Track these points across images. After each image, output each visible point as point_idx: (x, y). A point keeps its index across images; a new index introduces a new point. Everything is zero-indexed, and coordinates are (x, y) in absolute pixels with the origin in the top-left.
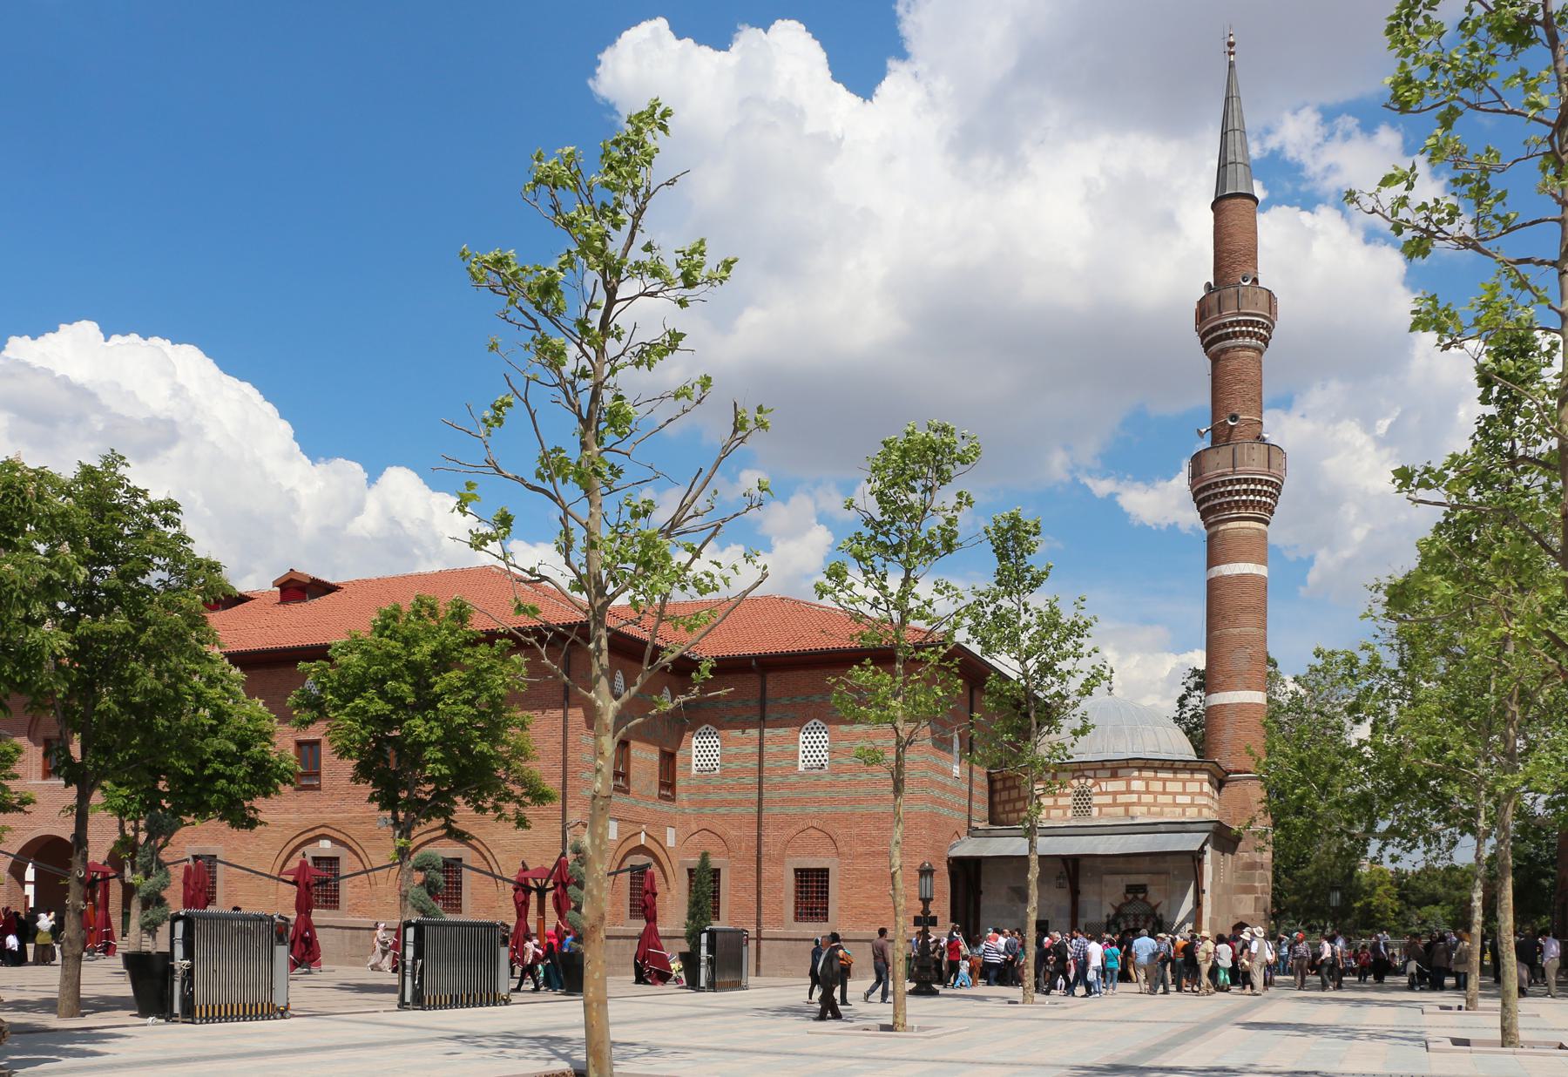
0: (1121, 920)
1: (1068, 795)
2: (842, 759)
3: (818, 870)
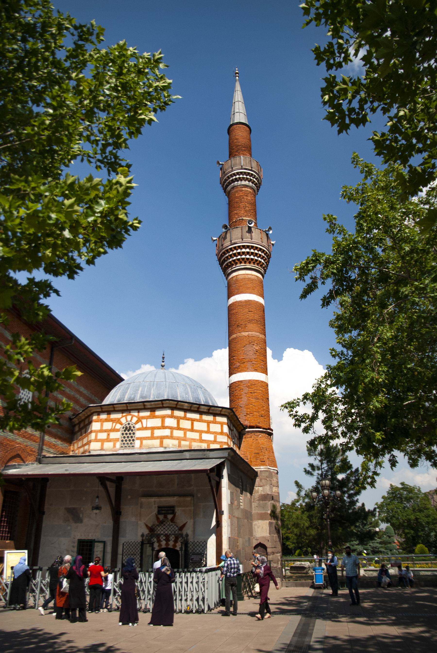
1: (118, 430)
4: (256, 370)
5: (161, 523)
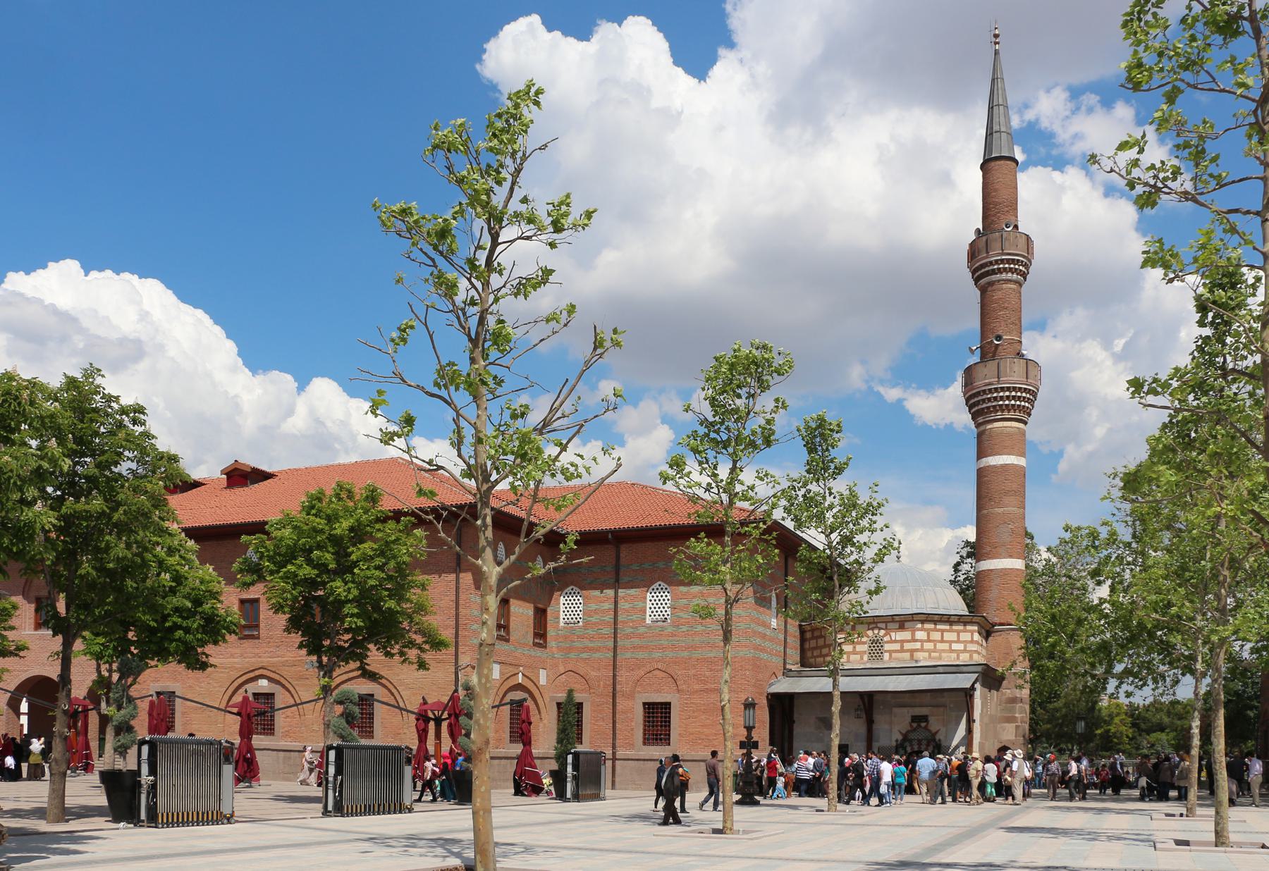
0: (907, 744)
1: (864, 643)
2: (681, 614)
3: (662, 704)
4: (1011, 557)
5: (915, 730)
